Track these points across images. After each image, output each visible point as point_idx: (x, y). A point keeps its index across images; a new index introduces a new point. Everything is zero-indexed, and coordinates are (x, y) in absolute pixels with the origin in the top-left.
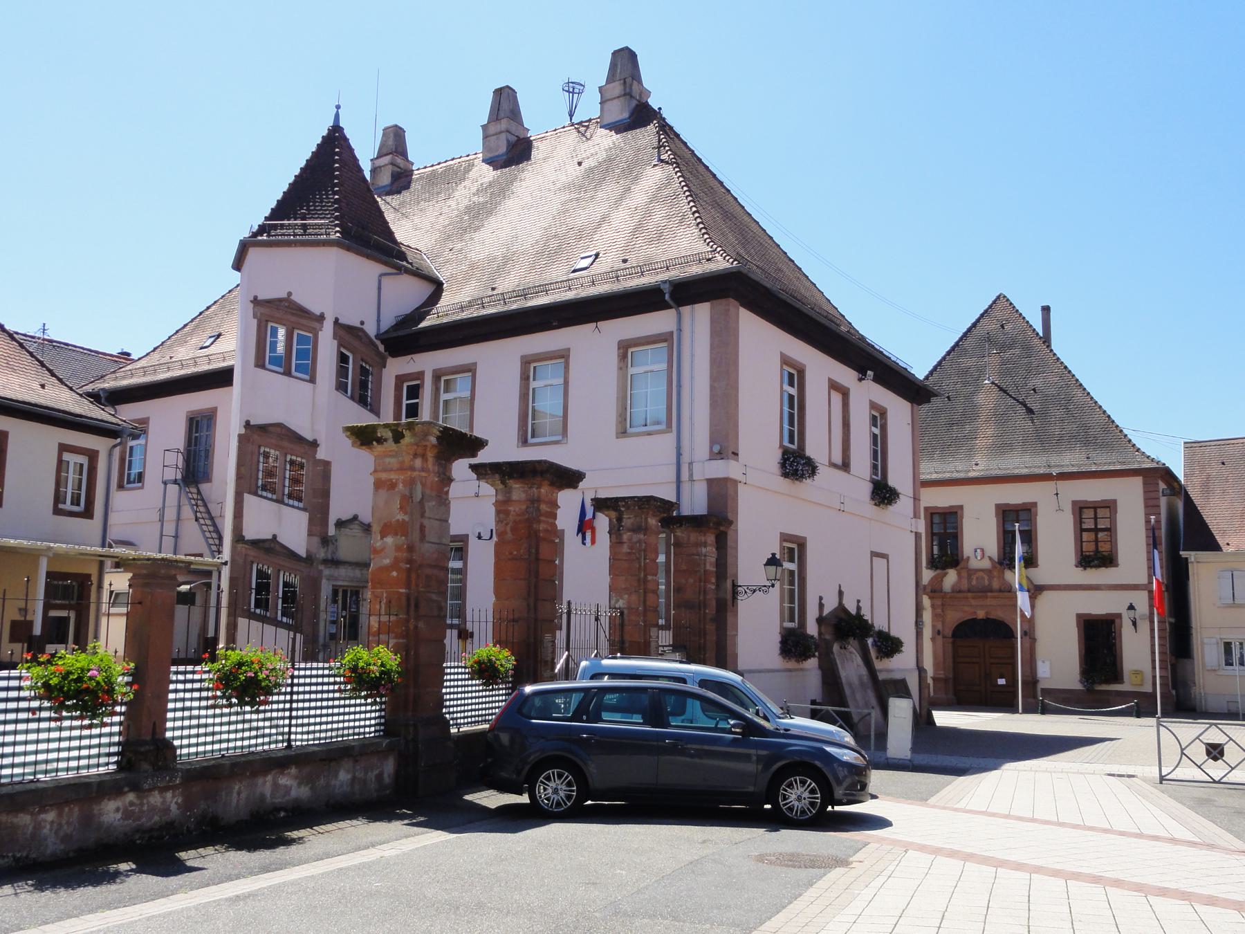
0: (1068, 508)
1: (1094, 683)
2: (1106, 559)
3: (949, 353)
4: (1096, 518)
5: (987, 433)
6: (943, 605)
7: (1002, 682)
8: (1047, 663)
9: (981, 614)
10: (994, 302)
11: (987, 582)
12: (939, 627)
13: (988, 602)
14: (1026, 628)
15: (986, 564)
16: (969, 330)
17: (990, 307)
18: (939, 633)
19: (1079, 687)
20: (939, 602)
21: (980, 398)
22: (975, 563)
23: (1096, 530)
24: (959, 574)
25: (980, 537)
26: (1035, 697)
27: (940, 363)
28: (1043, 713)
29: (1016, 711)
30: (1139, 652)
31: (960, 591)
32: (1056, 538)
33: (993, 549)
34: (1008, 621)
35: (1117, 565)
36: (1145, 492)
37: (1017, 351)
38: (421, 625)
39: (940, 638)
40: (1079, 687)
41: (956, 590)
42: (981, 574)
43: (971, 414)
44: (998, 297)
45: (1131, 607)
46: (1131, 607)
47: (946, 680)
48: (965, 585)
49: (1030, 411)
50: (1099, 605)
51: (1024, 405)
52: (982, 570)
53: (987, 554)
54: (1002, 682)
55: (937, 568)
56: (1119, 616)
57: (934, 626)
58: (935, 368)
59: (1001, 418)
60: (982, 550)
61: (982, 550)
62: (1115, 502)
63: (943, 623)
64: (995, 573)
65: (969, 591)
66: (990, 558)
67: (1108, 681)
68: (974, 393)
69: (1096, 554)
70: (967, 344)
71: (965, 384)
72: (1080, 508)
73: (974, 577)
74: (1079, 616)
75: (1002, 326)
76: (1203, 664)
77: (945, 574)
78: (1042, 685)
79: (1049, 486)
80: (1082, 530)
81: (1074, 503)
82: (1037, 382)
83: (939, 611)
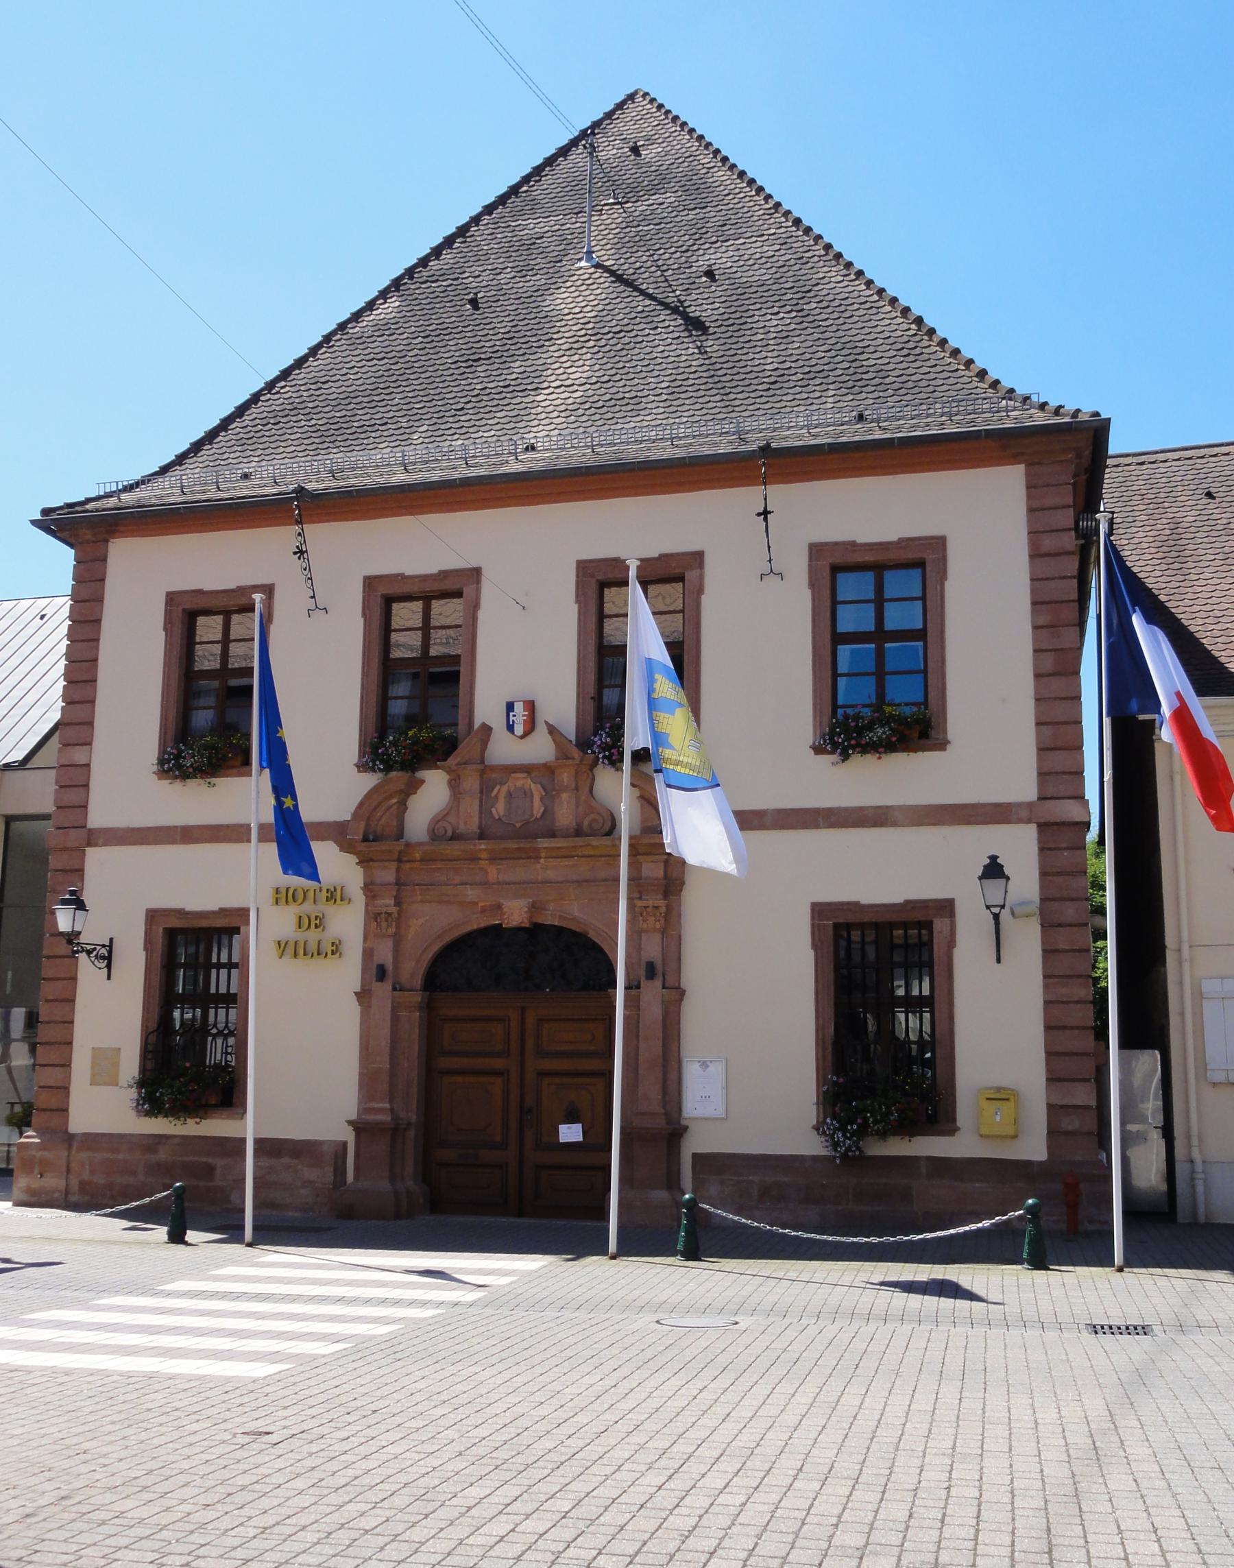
0: (798, 567)
1: (863, 1132)
2: (917, 729)
3: (489, 209)
4: (879, 602)
5: (567, 376)
6: (399, 883)
7: (570, 1133)
8: (716, 1069)
9: (516, 913)
10: (620, 106)
11: (538, 809)
12: (385, 954)
13: (546, 869)
14: (652, 949)
15: (540, 749)
16: (550, 161)
17: (609, 115)
18: (381, 973)
19: (812, 1145)
20: (387, 875)
21: (563, 300)
22: (506, 749)
23: (880, 635)
24: (454, 784)
25: (522, 665)
26: (672, 1182)
27: (463, 231)
28: (693, 1253)
29: (600, 1248)
30: (997, 1024)
31: (455, 837)
32: (765, 636)
33: (562, 702)
34: (592, 925)
35: (942, 745)
36: (1031, 510)
37: (670, 198)
38: (229, 1058)
39: (383, 991)
40: (812, 1145)
41: (442, 833)
42: (520, 780)
43: (532, 332)
44: (631, 97)
45: (994, 870)
46: (994, 870)
47: (396, 1131)
48: (469, 819)
49: (696, 325)
50: (880, 872)
51: (677, 310)
52: (528, 769)
53: (546, 713)
54: (570, 1133)
55: (388, 768)
56: (946, 907)
57: (368, 954)
58: (449, 241)
59: (606, 337)
60: (531, 706)
61: (531, 706)
62: (938, 544)
63: (398, 940)
64: (566, 777)
65: (482, 836)
66: (552, 730)
67: (910, 1127)
68: (541, 291)
69: (879, 697)
70: (538, 190)
71: (522, 272)
72: (835, 566)
73: (501, 791)
74: (820, 911)
75: (635, 150)
76: (1202, 1066)
77: (414, 786)
78: (697, 1143)
79: (742, 500)
80: (838, 638)
81: (816, 550)
82: (721, 258)
83: (386, 902)
